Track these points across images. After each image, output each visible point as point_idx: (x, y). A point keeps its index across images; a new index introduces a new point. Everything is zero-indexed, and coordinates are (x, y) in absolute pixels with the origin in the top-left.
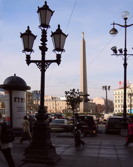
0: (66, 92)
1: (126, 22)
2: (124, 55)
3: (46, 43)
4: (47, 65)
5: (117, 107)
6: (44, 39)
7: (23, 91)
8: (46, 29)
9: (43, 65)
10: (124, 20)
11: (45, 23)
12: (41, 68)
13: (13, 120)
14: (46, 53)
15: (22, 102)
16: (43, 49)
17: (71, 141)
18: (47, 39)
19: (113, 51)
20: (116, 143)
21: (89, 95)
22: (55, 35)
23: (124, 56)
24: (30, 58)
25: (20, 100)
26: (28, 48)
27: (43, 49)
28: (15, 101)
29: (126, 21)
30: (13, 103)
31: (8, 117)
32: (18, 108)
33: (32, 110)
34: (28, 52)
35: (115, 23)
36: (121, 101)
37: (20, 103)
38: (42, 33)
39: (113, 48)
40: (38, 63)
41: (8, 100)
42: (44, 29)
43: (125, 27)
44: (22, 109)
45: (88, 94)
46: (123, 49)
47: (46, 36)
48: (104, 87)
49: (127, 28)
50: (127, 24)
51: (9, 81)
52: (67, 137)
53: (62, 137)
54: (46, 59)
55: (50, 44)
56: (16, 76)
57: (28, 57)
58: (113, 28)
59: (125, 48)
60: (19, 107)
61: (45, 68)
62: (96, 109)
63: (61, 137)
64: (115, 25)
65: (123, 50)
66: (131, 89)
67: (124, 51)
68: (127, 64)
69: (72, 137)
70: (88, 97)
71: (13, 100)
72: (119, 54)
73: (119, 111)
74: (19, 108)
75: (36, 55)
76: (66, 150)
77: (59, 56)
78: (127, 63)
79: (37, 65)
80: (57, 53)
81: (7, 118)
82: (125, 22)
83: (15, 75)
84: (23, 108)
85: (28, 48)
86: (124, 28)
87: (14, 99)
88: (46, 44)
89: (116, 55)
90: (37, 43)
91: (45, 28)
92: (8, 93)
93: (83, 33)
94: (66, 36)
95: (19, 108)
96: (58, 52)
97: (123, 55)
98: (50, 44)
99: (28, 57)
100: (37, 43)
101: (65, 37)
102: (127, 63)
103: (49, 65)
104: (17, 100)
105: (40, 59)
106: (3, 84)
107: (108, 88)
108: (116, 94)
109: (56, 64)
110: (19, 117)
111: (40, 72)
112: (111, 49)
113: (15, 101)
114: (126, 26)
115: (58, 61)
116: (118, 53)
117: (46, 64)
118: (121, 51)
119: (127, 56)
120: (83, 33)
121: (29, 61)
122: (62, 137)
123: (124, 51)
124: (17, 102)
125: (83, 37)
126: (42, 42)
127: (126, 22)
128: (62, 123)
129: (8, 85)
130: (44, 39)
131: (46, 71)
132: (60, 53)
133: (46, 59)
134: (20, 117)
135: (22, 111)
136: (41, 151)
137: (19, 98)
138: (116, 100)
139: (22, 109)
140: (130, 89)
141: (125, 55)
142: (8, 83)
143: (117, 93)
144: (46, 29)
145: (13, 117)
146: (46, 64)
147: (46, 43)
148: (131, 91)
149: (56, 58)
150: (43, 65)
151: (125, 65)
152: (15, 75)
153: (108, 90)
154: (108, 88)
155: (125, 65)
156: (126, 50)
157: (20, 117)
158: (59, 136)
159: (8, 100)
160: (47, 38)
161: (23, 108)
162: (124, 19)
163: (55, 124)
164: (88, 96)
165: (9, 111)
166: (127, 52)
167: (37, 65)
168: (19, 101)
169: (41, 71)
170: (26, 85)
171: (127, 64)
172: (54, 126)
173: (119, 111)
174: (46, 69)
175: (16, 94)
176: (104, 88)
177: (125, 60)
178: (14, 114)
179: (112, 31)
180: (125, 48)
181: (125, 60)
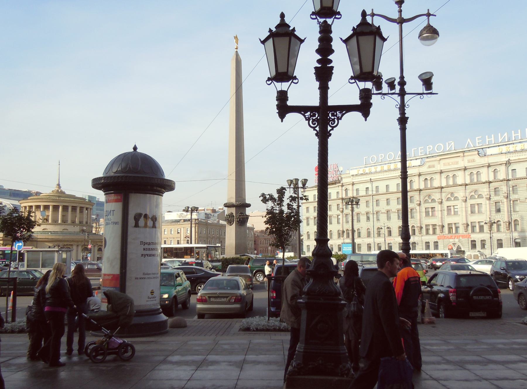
0: (263, 195)
1: (400, 11)
2: (399, 94)
3: (329, 58)
4: (334, 120)
5: (362, 235)
6: (325, 49)
7: (156, 196)
8: (329, 21)
9: (323, 117)
10: (397, 6)
11: (330, 5)
12: (317, 129)
13: (128, 284)
14: (329, 86)
15: (154, 226)
16: (324, 74)
17: (17, 343)
18: (333, 48)
19: (421, 83)
20: (225, 344)
21: (249, 205)
22: (277, 39)
23: (398, 99)
24: (286, 99)
25: (150, 223)
26: (283, 74)
27: (324, 74)
28: (137, 225)
29: (401, 7)
30: (131, 229)
31: (114, 275)
32: (143, 247)
33: (89, 251)
34: (277, 82)
35: (375, 12)
36: (365, 217)
37: (142, 230)
38: (320, 32)
39: (423, 76)
40: (309, 113)
41: (116, 223)
42: (325, 22)
43: (398, 23)
44: (152, 249)
45: (247, 202)
46: (398, 80)
47: (331, 40)
48: (292, 181)
49: (404, 25)
50: (405, 16)
51: (124, 165)
52: (268, 330)
53: (257, 330)
54: (332, 102)
55: (342, 62)
56: (138, 150)
57: (282, 96)
58: (425, 24)
59: (402, 77)
60: (145, 244)
61: (329, 128)
62: (255, 244)
63: (254, 331)
64: (375, 17)
65: (396, 83)
66: (344, 188)
67: (399, 84)
68: (408, 118)
69: (285, 330)
70: (248, 211)
71: (131, 222)
72: (387, 92)
73: (379, 248)
74: (146, 246)
75: (304, 91)
76: (197, 372)
77: (366, 95)
78: (406, 116)
79: (308, 119)
80: (363, 85)
81: (110, 277)
82: (399, 12)
83: (135, 148)
84: (151, 247)
85: (283, 74)
86: (396, 26)
87: (135, 218)
88: (319, 61)
89: (379, 96)
90: (307, 59)
91: (328, 20)
92: (116, 201)
93: (236, 38)
94: (302, 41)
95: (146, 246)
96: (363, 83)
97: (397, 95)
98: (342, 62)
99: (282, 96)
100: (307, 59)
101: (299, 43)
102: (406, 116)
103: (341, 119)
104: (142, 222)
105: (315, 102)
106: (102, 176)
107: (300, 185)
108: (388, 193)
109: (358, 115)
110: (144, 274)
111: (316, 140)
112: (420, 77)
113: (137, 225)
114: (401, 21)
115: (364, 108)
116: (385, 88)
117: (330, 115)
118: (391, 85)
119: (407, 97)
120: (236, 38)
121: (284, 108)
122: (257, 330)
123: (399, 84)
124: (149, 227)
125: (237, 48)
126: (320, 57)
127: (400, 11)
128: (232, 288)
129: (115, 177)
130: (325, 49)
131: (330, 135)
132: (284, 86)
133: (332, 102)
134: (147, 274)
135: (150, 255)
136: (337, 378)
137: (146, 216)
138: (308, 218)
139: (152, 249)
140: (342, 186)
141: (402, 94)
142: (122, 171)
143: (382, 190)
144: (329, 21)
145: (128, 275)
146: (330, 115)
147: (329, 58)
148: (344, 192)
149: (360, 99)
150: (323, 117)
151: (403, 121)
152: (135, 148)
153: (302, 190)
154: (300, 185)
155: (403, 121)
156: (402, 83)
157: (147, 274)
158: (247, 329)
159: (116, 223)
160: (332, 44)
161: (151, 247)
162: (396, 3)
163: (218, 292)
164: (247, 209)
165: (118, 256)
166: (405, 87)
167: (306, 120)
168: (146, 226)
169: (317, 135)
170: (162, 173)
171: (408, 118)
172: (214, 297)
173: (379, 248)
174: (333, 128)
175: (139, 203)
176: (292, 186)
177: (402, 108)
178: (130, 265)
179: (425, 32)
180: (402, 77)
181: (402, 108)
